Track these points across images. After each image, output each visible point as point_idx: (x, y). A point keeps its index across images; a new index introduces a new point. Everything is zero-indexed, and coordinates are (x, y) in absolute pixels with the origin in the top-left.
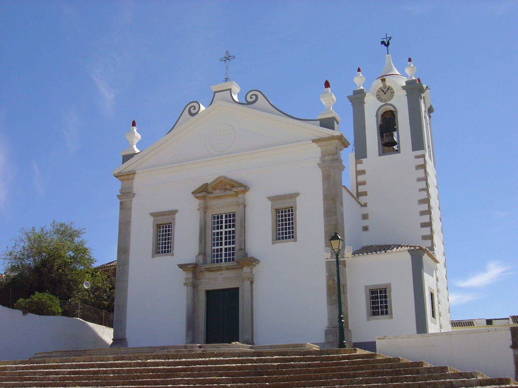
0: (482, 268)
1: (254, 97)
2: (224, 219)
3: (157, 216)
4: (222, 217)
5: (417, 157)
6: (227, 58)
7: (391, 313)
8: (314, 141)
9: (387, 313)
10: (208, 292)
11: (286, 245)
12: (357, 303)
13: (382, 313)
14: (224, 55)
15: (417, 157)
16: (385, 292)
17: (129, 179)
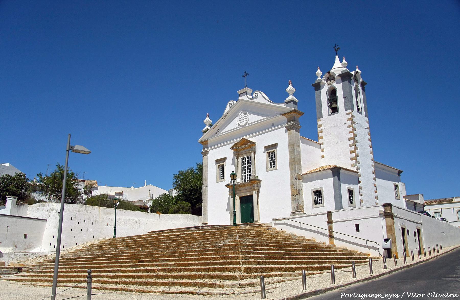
0: (138, 185)
3: (406, 254)
5: (347, 114)
6: (245, 75)
8: (282, 115)
11: (273, 173)
14: (243, 74)
15: (347, 114)
16: (321, 192)
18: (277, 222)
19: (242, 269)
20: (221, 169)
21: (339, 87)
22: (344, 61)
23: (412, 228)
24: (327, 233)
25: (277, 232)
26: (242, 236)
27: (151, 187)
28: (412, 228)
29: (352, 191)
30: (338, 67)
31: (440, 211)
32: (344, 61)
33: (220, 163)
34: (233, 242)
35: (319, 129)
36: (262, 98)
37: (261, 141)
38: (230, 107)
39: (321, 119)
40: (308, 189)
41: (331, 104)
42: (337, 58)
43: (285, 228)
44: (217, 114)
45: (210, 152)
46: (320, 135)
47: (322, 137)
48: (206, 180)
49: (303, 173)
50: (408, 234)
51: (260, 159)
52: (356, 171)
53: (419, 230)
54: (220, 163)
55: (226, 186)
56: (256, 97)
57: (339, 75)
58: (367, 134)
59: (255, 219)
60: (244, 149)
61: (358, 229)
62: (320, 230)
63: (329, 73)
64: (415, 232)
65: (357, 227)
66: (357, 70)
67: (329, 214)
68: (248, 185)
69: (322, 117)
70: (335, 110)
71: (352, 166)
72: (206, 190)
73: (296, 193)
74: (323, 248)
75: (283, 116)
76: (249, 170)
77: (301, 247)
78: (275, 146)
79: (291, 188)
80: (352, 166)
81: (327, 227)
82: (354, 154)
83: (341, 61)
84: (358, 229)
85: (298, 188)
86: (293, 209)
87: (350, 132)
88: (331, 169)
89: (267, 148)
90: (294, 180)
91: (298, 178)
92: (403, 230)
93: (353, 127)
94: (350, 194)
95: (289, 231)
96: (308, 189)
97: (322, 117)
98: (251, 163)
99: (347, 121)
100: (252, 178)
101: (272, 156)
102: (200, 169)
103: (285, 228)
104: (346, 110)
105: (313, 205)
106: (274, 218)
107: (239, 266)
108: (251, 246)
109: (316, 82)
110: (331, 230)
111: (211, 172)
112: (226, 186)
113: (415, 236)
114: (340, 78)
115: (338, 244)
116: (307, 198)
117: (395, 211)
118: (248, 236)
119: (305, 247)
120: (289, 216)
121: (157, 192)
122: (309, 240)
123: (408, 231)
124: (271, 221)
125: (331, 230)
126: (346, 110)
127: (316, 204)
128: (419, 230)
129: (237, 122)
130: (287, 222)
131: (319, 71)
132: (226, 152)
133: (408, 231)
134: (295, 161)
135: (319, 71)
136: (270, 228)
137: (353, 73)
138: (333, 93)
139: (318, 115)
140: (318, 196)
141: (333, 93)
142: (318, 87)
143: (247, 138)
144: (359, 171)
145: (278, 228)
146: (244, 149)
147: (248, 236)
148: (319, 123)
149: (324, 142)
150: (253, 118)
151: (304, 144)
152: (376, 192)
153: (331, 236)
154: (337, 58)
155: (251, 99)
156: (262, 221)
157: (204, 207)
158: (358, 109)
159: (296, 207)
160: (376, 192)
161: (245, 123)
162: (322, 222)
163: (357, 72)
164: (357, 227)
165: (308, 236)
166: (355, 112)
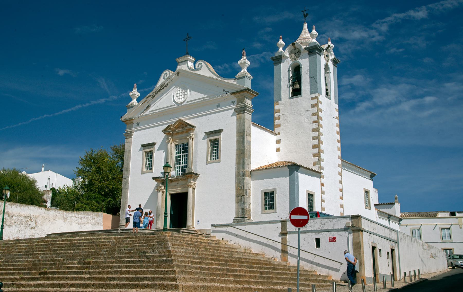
1: (200, 65)
2: (182, 147)
3: (145, 146)
4: (181, 146)
5: (313, 98)
7: (276, 209)
8: (232, 94)
9: (273, 209)
10: (172, 196)
11: (215, 165)
12: (255, 202)
13: (271, 209)
15: (313, 98)
17: (130, 123)
18: (217, 229)
19: (180, 286)
20: (149, 156)
21: (305, 63)
22: (314, 31)
23: (385, 246)
24: (279, 246)
25: (217, 242)
26: (176, 245)
27: (50, 173)
28: (385, 246)
29: (312, 195)
30: (308, 37)
31: (418, 227)
32: (314, 31)
33: (148, 150)
34: (164, 252)
35: (276, 115)
36: (206, 70)
37: (202, 124)
38: (164, 78)
39: (280, 102)
40: (255, 189)
41: (294, 84)
42: (306, 25)
43: (227, 237)
44: (149, 89)
45: (135, 134)
46: (277, 122)
47: (279, 126)
48: (128, 170)
49: (252, 169)
50: (380, 256)
51: (199, 147)
52: (319, 171)
53: (392, 250)
54: (148, 150)
55: (154, 178)
56: (200, 69)
57: (306, 49)
58: (336, 125)
59: (189, 223)
60: (180, 132)
61: (318, 245)
62: (270, 243)
63: (294, 44)
64: (388, 253)
65: (318, 241)
66: (330, 43)
67: (284, 223)
68: (182, 180)
69: (281, 100)
70: (296, 92)
71: (315, 164)
72: (127, 183)
73: (241, 194)
74: (274, 265)
75: (233, 96)
76: (186, 159)
77: (247, 262)
78: (219, 132)
79: (237, 187)
80: (315, 164)
81: (279, 239)
82: (318, 149)
83: (310, 31)
84: (318, 245)
85: (245, 188)
86: (237, 213)
87: (314, 122)
88: (288, 166)
89: (209, 134)
90: (240, 177)
91: (242, 173)
92: (374, 248)
93: (318, 115)
94: (309, 200)
95: (232, 241)
96: (255, 189)
97: (281, 100)
98: (187, 152)
99: (312, 107)
100: (187, 171)
101: (215, 144)
102: (121, 154)
103: (227, 237)
104: (311, 93)
105: (262, 210)
106: (215, 223)
107: (175, 282)
108: (187, 258)
109: (277, 54)
110: (284, 243)
111: (135, 159)
112: (154, 178)
113: (388, 258)
114: (307, 52)
115: (305, 266)
116: (255, 202)
117: (364, 225)
118: (182, 246)
119: (252, 263)
120: (231, 222)
121: (63, 182)
122: (257, 254)
123: (380, 250)
124: (210, 227)
125: (284, 243)
126: (311, 93)
127: (266, 209)
128: (392, 250)
129: (172, 97)
130: (230, 229)
131: (281, 41)
132: (155, 134)
133: (380, 250)
134: (242, 153)
135: (281, 41)
136: (208, 236)
137: (324, 47)
138: (297, 70)
139: (275, 98)
140: (269, 199)
141: (297, 70)
142: (279, 60)
143: (182, 118)
144: (322, 171)
145: (218, 237)
146: (180, 132)
147: (182, 246)
148: (276, 107)
149: (281, 132)
150: (193, 96)
151: (303, 175)
152: (341, 198)
153: (284, 252)
154: (306, 25)
155: (193, 70)
156: (196, 227)
157: (123, 205)
158: (327, 94)
159: (241, 210)
160: (341, 198)
161: (183, 100)
162: (274, 232)
163: (329, 46)
164: (318, 241)
165: (255, 249)
166: (322, 97)
